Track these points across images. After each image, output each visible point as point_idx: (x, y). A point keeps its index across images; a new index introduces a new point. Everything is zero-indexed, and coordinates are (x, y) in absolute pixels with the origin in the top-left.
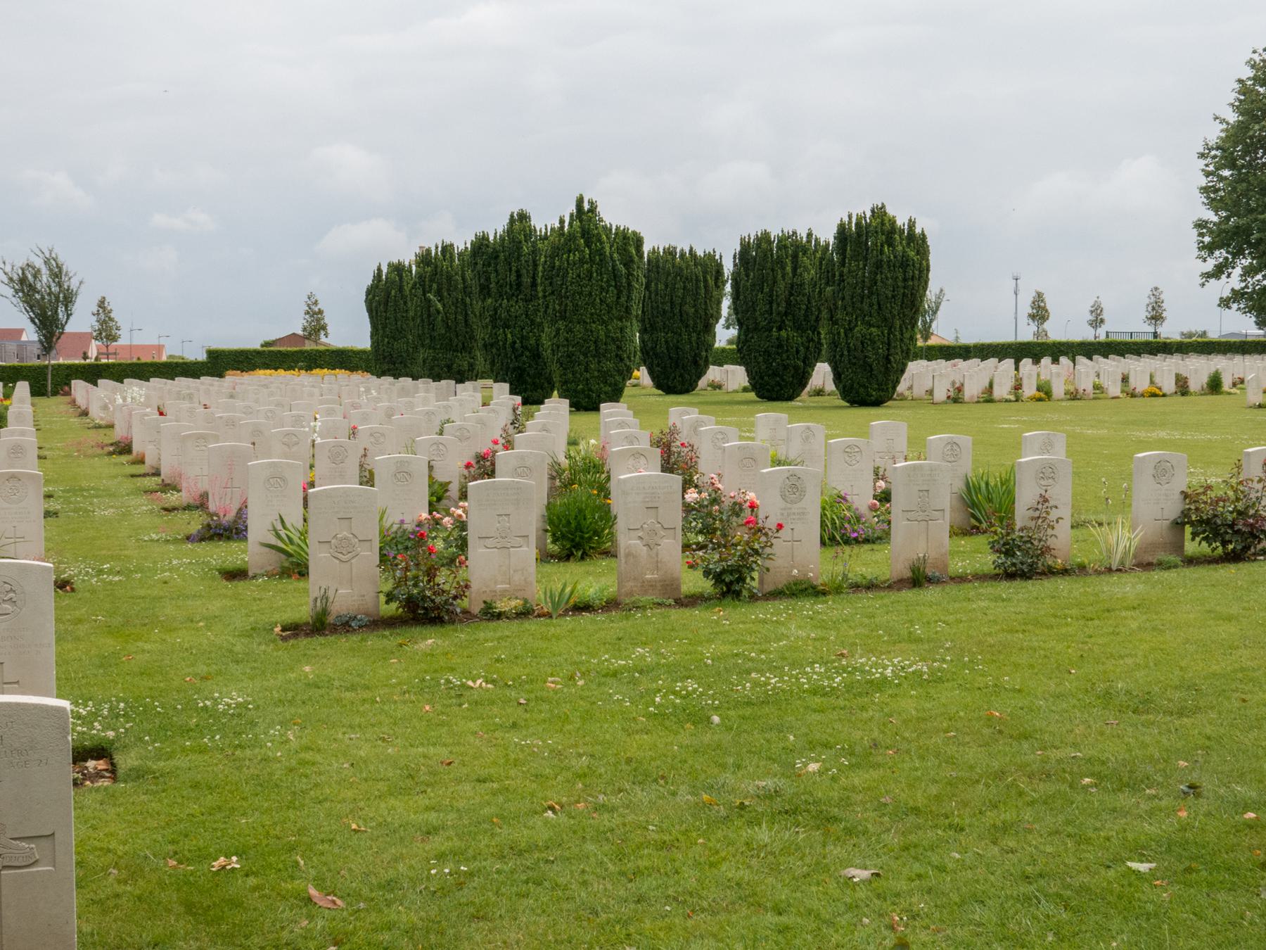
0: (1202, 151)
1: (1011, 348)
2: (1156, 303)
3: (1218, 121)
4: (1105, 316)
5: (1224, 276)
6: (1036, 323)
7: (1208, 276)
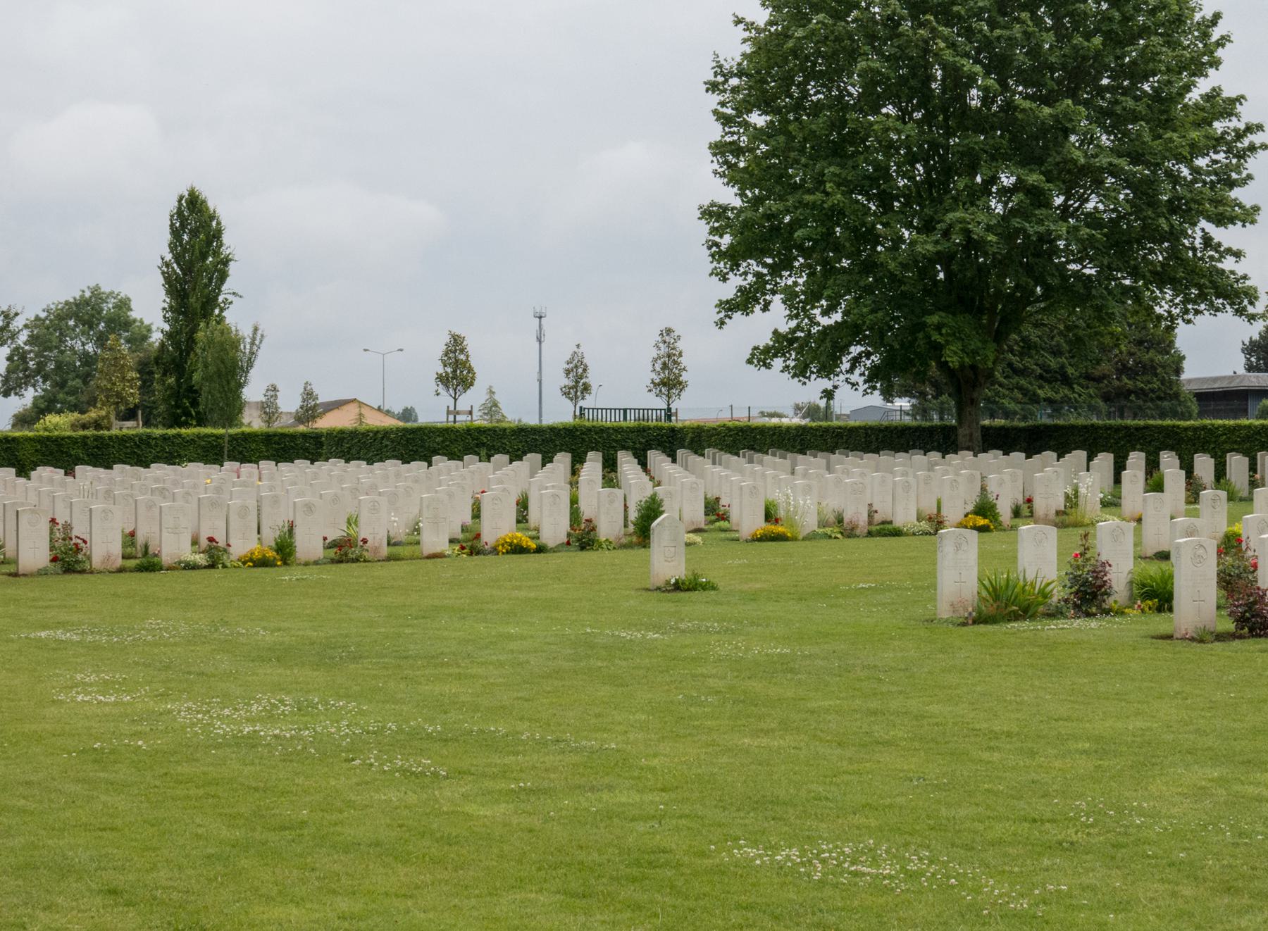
0: (712, 78)
1: (389, 439)
2: (669, 356)
3: (741, 26)
4: (592, 378)
5: (757, 308)
6: (451, 391)
7: (729, 307)
